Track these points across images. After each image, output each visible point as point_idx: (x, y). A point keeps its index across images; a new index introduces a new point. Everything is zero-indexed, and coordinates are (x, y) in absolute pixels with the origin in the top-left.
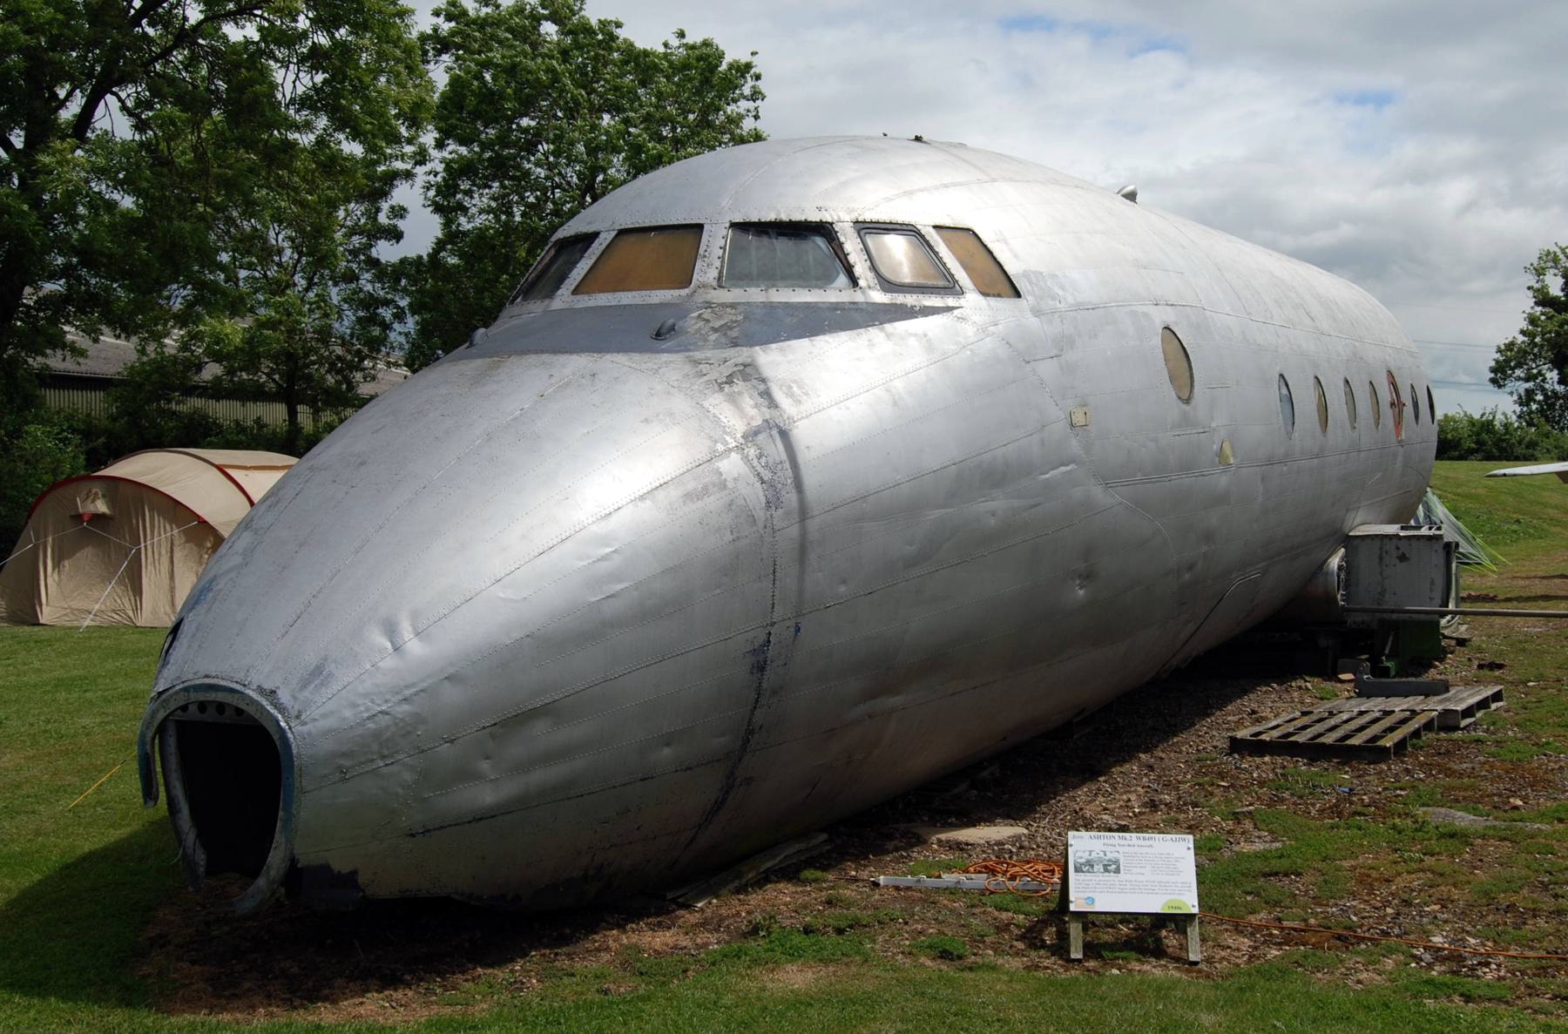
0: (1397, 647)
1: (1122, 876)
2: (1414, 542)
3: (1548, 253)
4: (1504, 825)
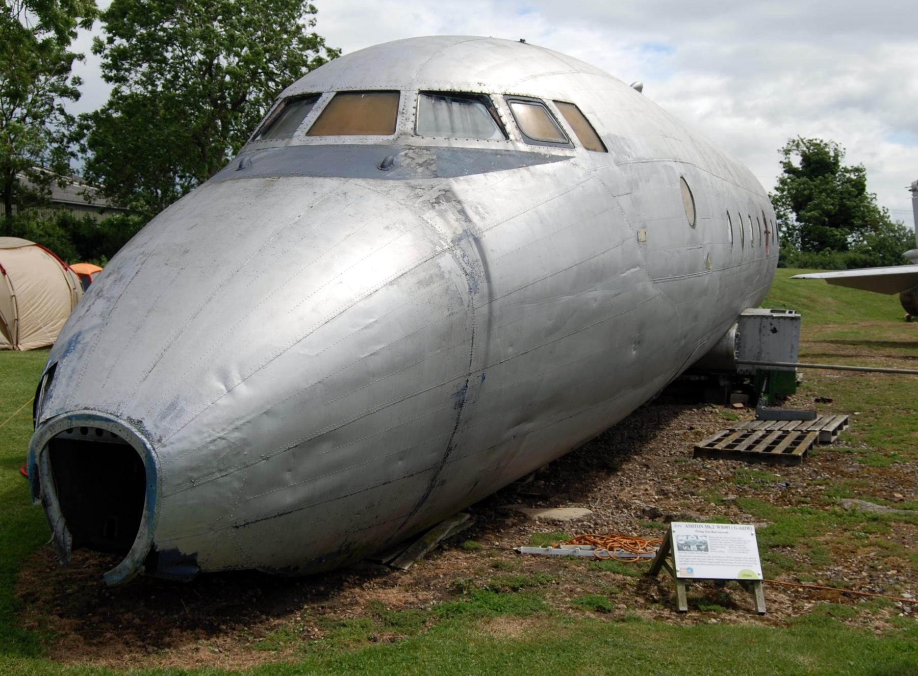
0: (758, 384)
1: (710, 553)
2: (782, 320)
3: (794, 141)
4: (902, 512)
